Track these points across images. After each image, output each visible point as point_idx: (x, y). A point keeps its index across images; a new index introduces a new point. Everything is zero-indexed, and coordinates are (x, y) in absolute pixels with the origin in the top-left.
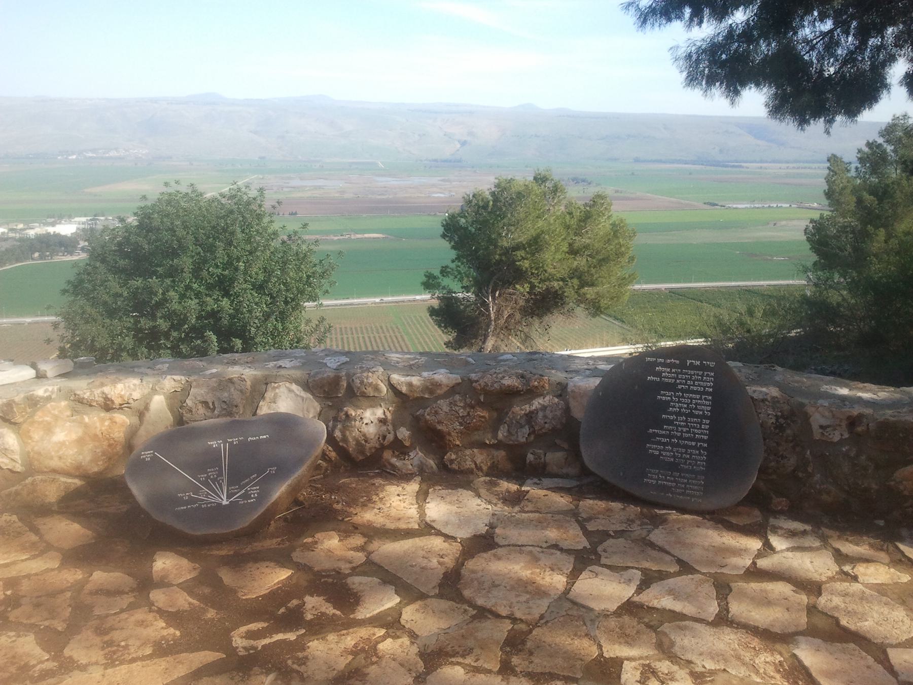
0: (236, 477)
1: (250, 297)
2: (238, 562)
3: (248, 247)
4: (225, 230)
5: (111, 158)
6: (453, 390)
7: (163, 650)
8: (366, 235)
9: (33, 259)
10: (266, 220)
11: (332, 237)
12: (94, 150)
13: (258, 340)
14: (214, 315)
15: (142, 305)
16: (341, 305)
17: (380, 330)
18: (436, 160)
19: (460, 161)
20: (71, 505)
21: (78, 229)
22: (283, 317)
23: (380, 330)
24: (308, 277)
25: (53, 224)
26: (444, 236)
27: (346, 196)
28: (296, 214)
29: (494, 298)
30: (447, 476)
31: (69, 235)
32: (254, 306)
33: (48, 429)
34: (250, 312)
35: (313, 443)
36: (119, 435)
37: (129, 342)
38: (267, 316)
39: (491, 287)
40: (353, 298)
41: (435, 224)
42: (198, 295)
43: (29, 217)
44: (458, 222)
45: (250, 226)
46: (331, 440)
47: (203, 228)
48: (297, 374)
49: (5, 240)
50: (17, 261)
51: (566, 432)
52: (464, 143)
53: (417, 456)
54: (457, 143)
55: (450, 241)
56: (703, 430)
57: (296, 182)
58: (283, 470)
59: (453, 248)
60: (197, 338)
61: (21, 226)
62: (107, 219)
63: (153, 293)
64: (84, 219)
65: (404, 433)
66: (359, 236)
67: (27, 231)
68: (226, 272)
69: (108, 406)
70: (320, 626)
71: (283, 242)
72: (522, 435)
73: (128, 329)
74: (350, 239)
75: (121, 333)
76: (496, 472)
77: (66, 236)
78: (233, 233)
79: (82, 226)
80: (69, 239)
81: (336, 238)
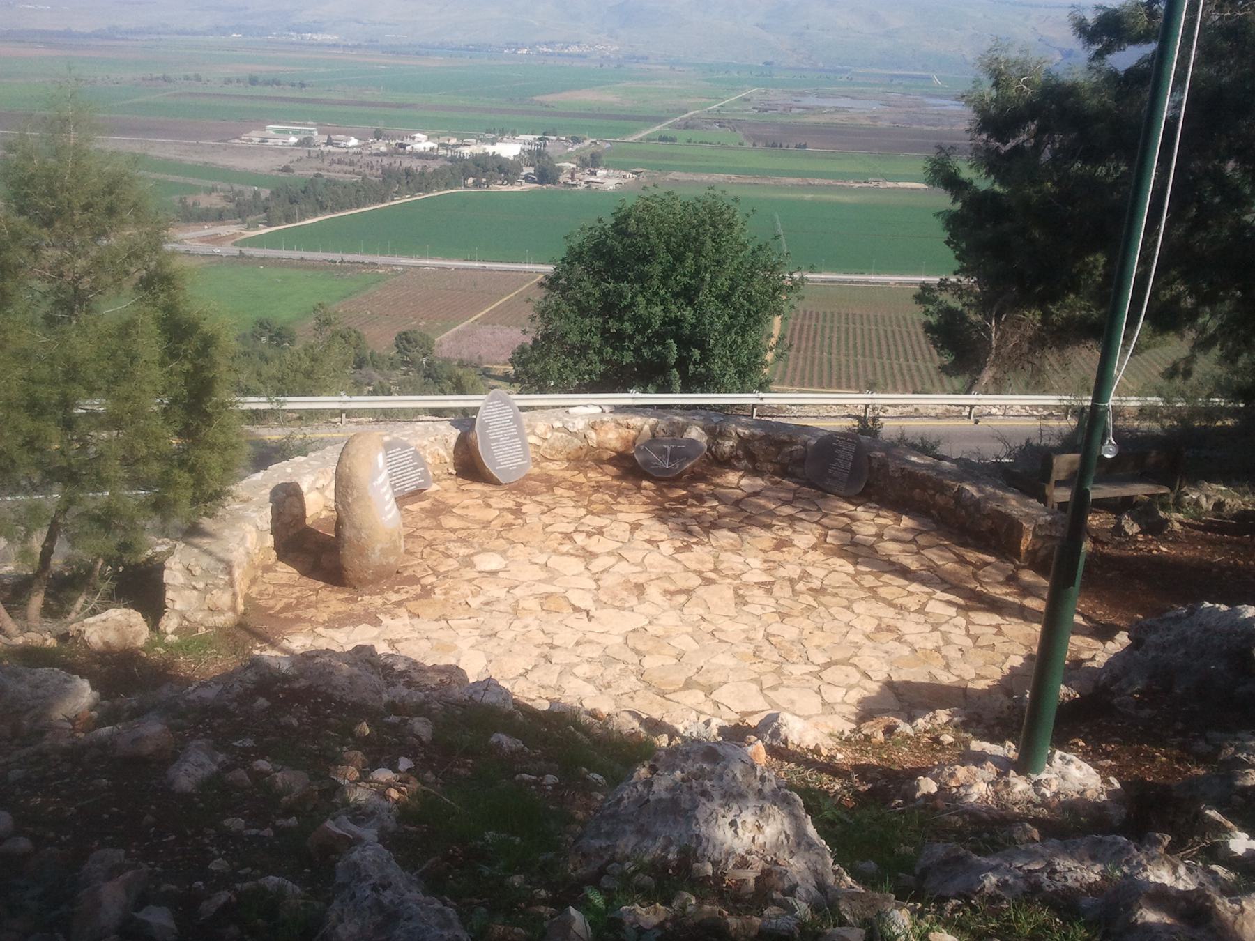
0: (672, 459)
1: (712, 307)
2: (669, 487)
3: (717, 257)
4: (696, 240)
5: (569, 55)
6: (762, 438)
7: (645, 504)
8: (901, 184)
9: (466, 186)
10: (736, 229)
11: (852, 183)
12: (549, 44)
13: (716, 352)
14: (677, 322)
15: (611, 308)
16: (852, 282)
17: (902, 322)
20: (611, 461)
21: (522, 150)
22: (743, 331)
23: (902, 322)
24: (775, 290)
25: (493, 142)
27: (880, 124)
28: (805, 146)
29: (998, 322)
30: (755, 472)
31: (511, 158)
32: (716, 319)
33: (607, 433)
34: (711, 323)
35: (702, 449)
36: (631, 438)
37: (597, 341)
38: (728, 329)
39: (995, 309)
40: (870, 274)
42: (663, 301)
43: (468, 129)
45: (720, 235)
46: (709, 449)
47: (675, 237)
48: (701, 423)
49: (435, 158)
50: (447, 186)
51: (800, 461)
53: (744, 462)
55: (955, 248)
56: (848, 466)
57: (811, 101)
58: (689, 458)
59: (958, 258)
60: (659, 344)
61: (454, 141)
62: (558, 139)
63: (621, 296)
64: (530, 138)
65: (740, 452)
67: (461, 148)
68: (693, 282)
69: (628, 427)
70: (692, 505)
71: (754, 252)
72: (787, 460)
73: (597, 328)
74: (876, 189)
75: (590, 331)
76: (775, 473)
77: (506, 159)
78: (703, 243)
79: (528, 147)
80: (512, 162)
81: (857, 185)
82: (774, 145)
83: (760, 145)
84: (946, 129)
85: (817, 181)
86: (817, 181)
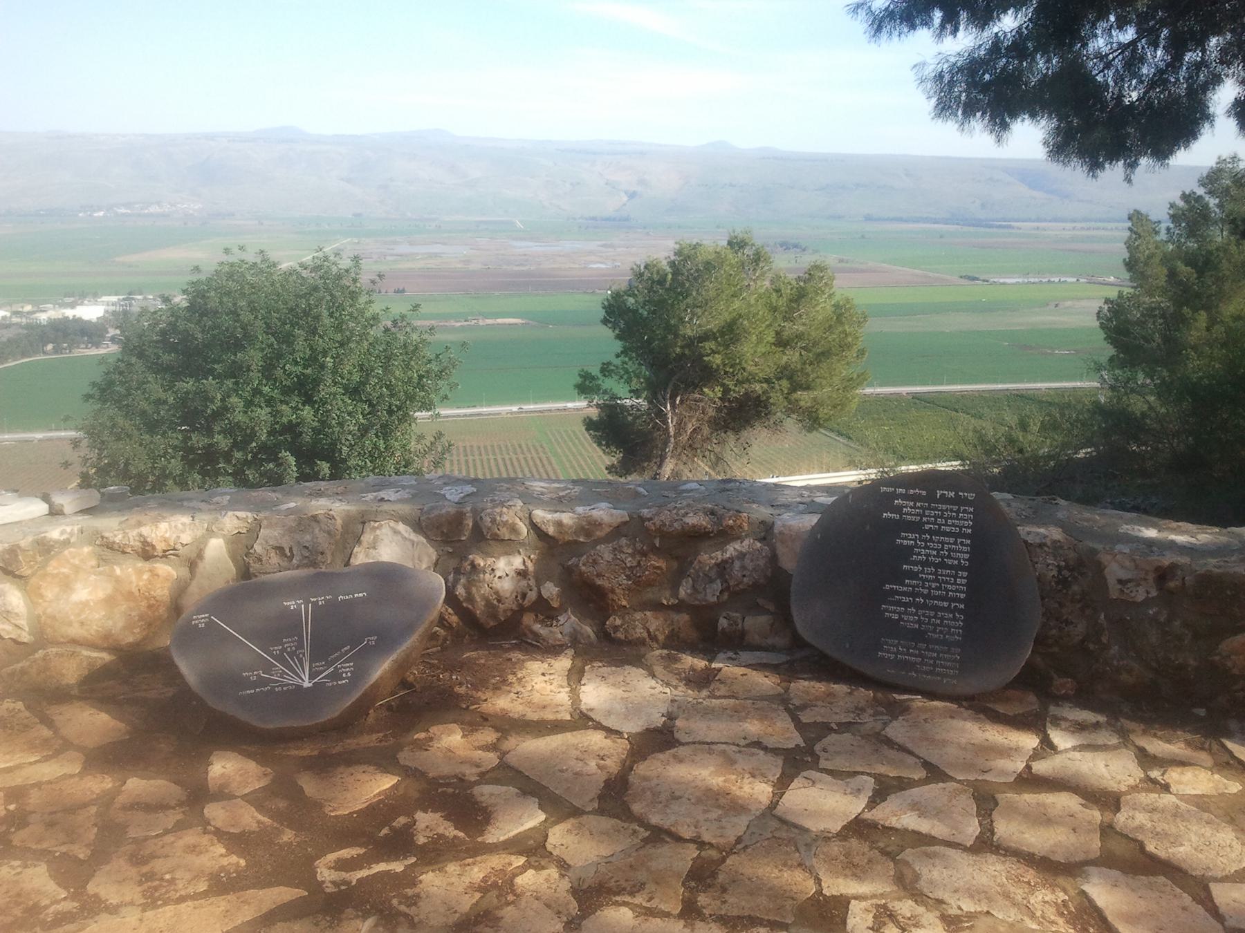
0: (322, 650)
1: (341, 405)
2: (324, 765)
3: (338, 337)
4: (306, 313)
5: (151, 215)
6: (618, 531)
7: (222, 885)
8: (500, 321)
9: (45, 353)
10: (363, 299)
11: (453, 323)
12: (128, 205)
13: (352, 463)
14: (292, 429)
15: (193, 415)
16: (465, 415)
17: (519, 450)
18: (594, 219)
19: (627, 219)
20: (97, 687)
21: (106, 311)
22: (386, 431)
23: (519, 450)
24: (421, 377)
25: (72, 306)
26: (605, 322)
27: (472, 267)
28: (403, 291)
29: (673, 406)
30: (610, 648)
31: (94, 320)
32: (347, 417)
33: (66, 585)
34: (341, 424)
35: (426, 604)
36: (162, 592)
37: (176, 465)
38: (364, 431)
39: (669, 391)
40: (482, 406)
41: (594, 305)
42: (270, 402)
43: (40, 295)
44: (624, 302)
45: (341, 307)
46: (451, 599)
47: (277, 311)
48: (405, 509)
49: (7, 326)
50: (24, 355)
51: (772, 589)
52: (632, 195)
53: (569, 621)
54: (623, 194)
55: (614, 329)
56: (958, 586)
57: (404, 249)
58: (386, 641)
59: (618, 337)
60: (268, 461)
61: (28, 308)
62: (145, 299)
63: (208, 399)
64: (114, 299)
65: (551, 590)
66: (489, 321)
67: (37, 315)
68: (309, 371)
69: (147, 553)
70: (436, 853)
71: (387, 330)
72: (712, 593)
73: (175, 448)
74: (477, 326)
75: (166, 453)
76: (676, 643)
77: (89, 322)
78: (317, 318)
79: (112, 308)
80: (95, 325)
81: (458, 324)
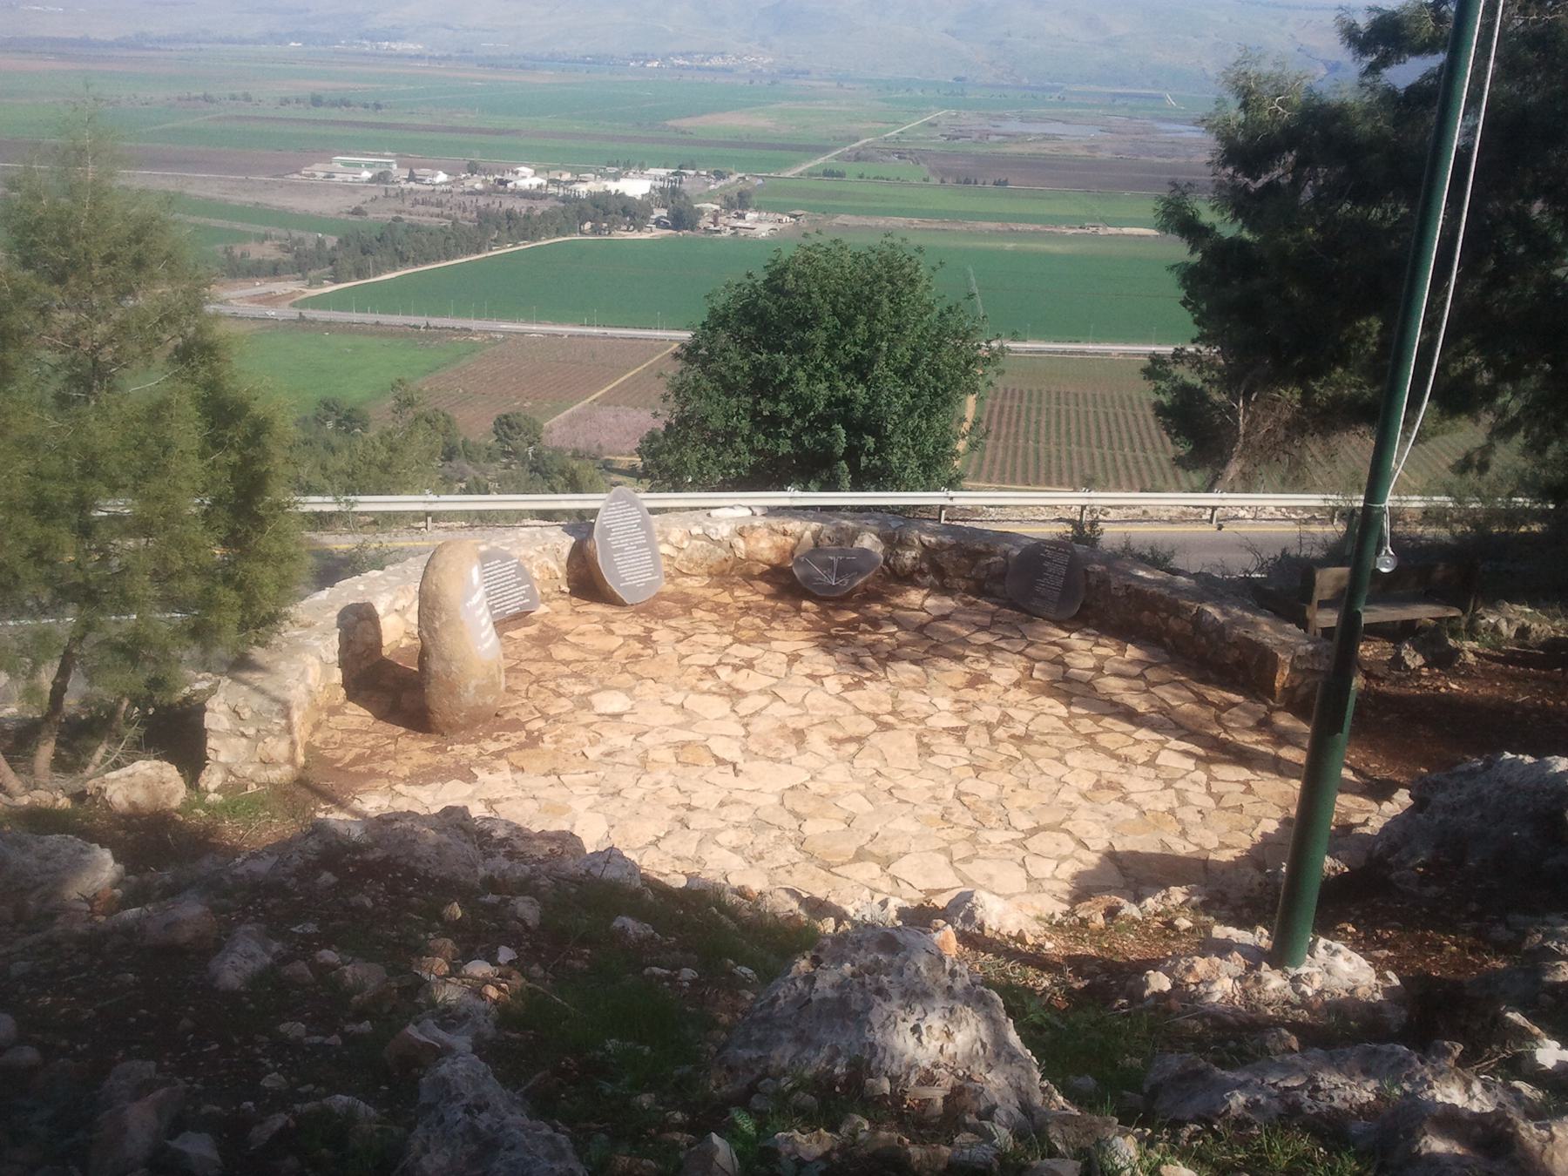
0: (840, 573)
1: (890, 384)
2: (836, 609)
3: (895, 321)
4: (870, 299)
5: (711, 69)
6: (952, 547)
7: (805, 629)
8: (1126, 230)
9: (582, 233)
10: (920, 287)
11: (1064, 229)
12: (686, 55)
13: (895, 439)
14: (846, 402)
15: (763, 384)
16: (1064, 352)
17: (1127, 403)
20: (763, 576)
21: (653, 187)
22: (929, 413)
23: (1127, 403)
24: (968, 363)
25: (616, 177)
27: (1099, 155)
28: (1005, 183)
29: (1246, 403)
30: (943, 590)
31: (639, 198)
32: (894, 399)
33: (758, 541)
34: (889, 404)
35: (877, 561)
36: (788, 548)
37: (746, 426)
38: (909, 411)
39: (1243, 386)
40: (1087, 342)
42: (829, 376)
43: (584, 161)
45: (900, 294)
46: (886, 561)
47: (844, 296)
48: (876, 529)
49: (544, 197)
50: (559, 232)
51: (1000, 577)
53: (930, 578)
55: (1193, 311)
56: (1060, 582)
57: (1013, 126)
58: (861, 572)
59: (1197, 322)
60: (823, 430)
61: (567, 176)
62: (698, 174)
63: (776, 370)
64: (663, 172)
65: (925, 566)
67: (576, 185)
68: (865, 352)
69: (785, 533)
70: (864, 632)
71: (941, 315)
72: (983, 575)
73: (745, 410)
74: (1095, 236)
75: (738, 414)
76: (968, 591)
77: (633, 199)
78: (879, 304)
79: (659, 184)
80: (640, 203)
81: (1071, 231)
82: (967, 182)
83: (949, 181)
84: (1182, 161)
85: (1020, 227)
86: (1020, 227)
